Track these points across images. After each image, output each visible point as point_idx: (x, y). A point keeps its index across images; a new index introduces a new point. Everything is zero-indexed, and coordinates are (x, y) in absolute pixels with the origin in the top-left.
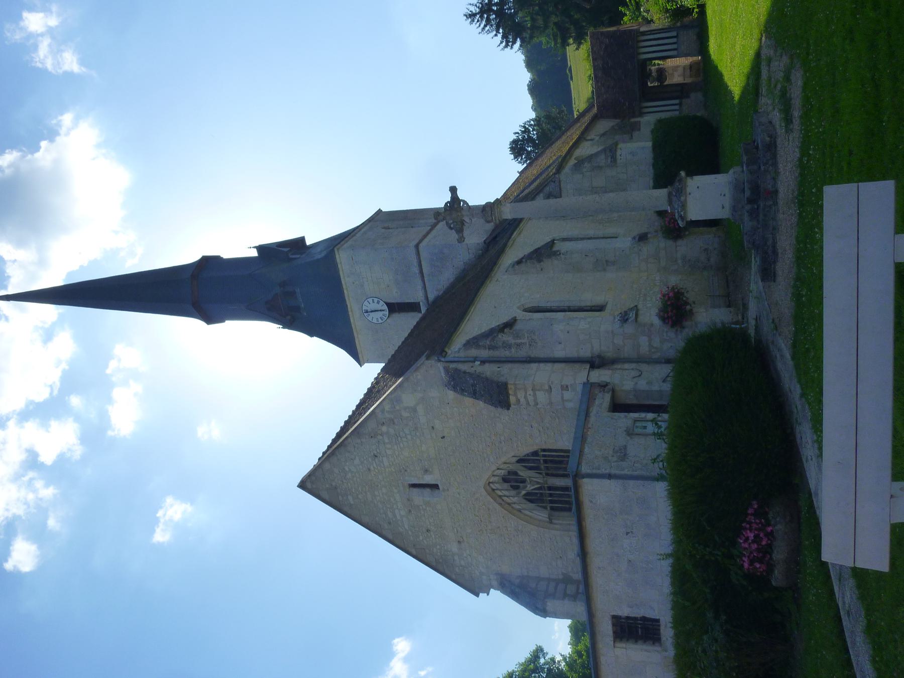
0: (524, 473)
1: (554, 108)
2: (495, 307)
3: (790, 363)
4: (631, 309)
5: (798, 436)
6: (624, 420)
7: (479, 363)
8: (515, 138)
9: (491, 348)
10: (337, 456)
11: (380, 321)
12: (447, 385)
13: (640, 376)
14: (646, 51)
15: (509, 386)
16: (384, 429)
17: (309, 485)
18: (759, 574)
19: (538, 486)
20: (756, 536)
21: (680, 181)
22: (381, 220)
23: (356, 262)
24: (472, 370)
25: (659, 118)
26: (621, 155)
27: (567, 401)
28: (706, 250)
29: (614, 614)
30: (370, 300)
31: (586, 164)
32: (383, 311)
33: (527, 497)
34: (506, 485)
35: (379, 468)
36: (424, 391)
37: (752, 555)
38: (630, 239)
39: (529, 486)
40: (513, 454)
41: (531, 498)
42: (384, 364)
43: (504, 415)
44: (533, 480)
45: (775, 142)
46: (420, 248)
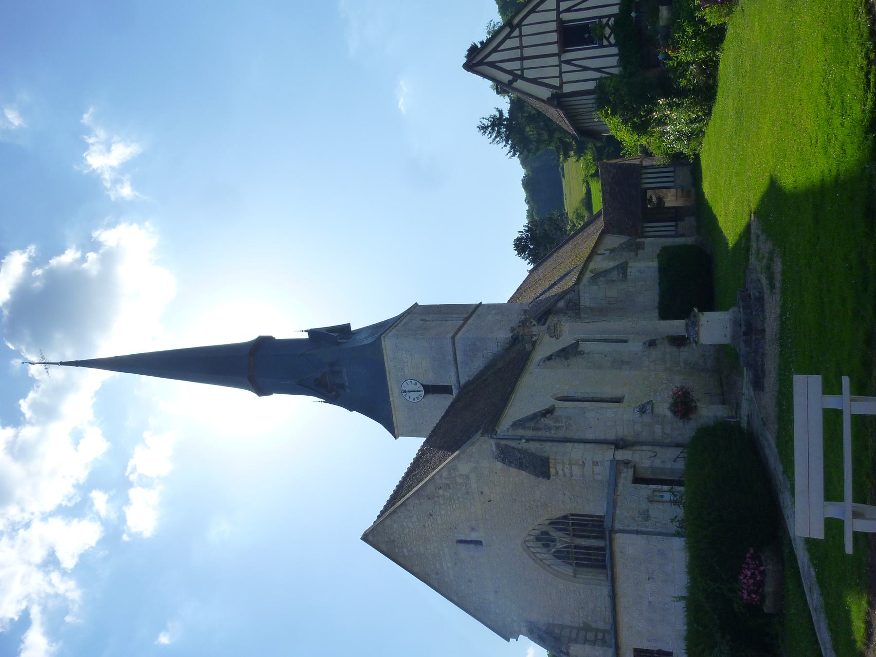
0: (555, 534)
1: (555, 211)
2: (532, 396)
3: (776, 450)
4: (648, 403)
5: (781, 502)
6: (646, 490)
7: (525, 440)
8: (520, 236)
9: (535, 429)
10: (398, 513)
11: (416, 400)
12: (497, 458)
13: (655, 456)
14: (648, 181)
15: (550, 461)
16: (441, 492)
17: (370, 538)
18: (754, 603)
19: (567, 545)
20: (753, 574)
21: (695, 316)
22: (415, 310)
23: (399, 349)
24: (519, 447)
25: (664, 246)
26: (631, 272)
27: (596, 474)
28: (704, 356)
29: (636, 647)
30: (409, 382)
31: (602, 278)
32: (419, 391)
33: (556, 554)
34: (539, 544)
35: (433, 525)
36: (477, 462)
37: (749, 588)
38: (641, 343)
39: (558, 544)
40: (547, 518)
41: (559, 555)
42: (424, 439)
43: (543, 483)
44: (562, 540)
45: (763, 297)
46: (455, 339)
